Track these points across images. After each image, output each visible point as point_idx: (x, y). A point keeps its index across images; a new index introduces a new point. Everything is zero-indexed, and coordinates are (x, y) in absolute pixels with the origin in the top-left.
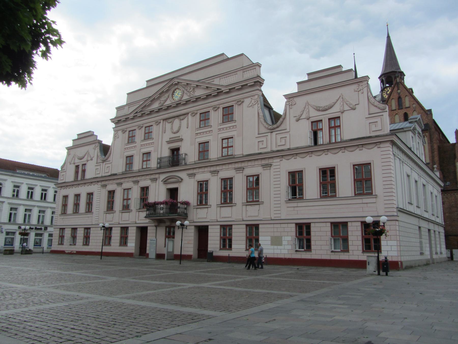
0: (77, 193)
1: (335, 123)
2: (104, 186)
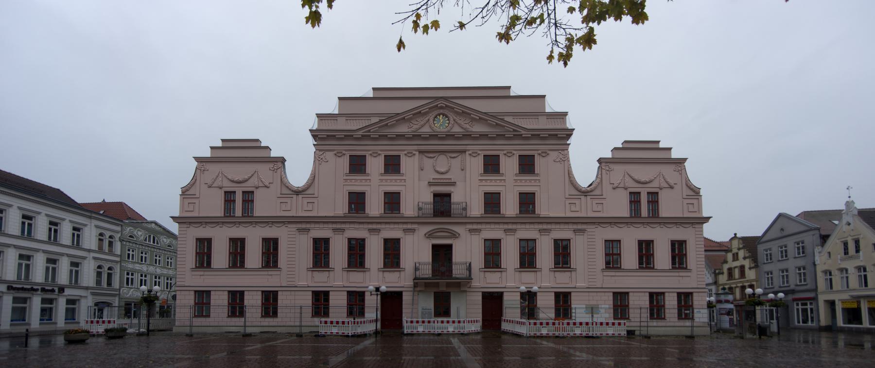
1: (248, 198)
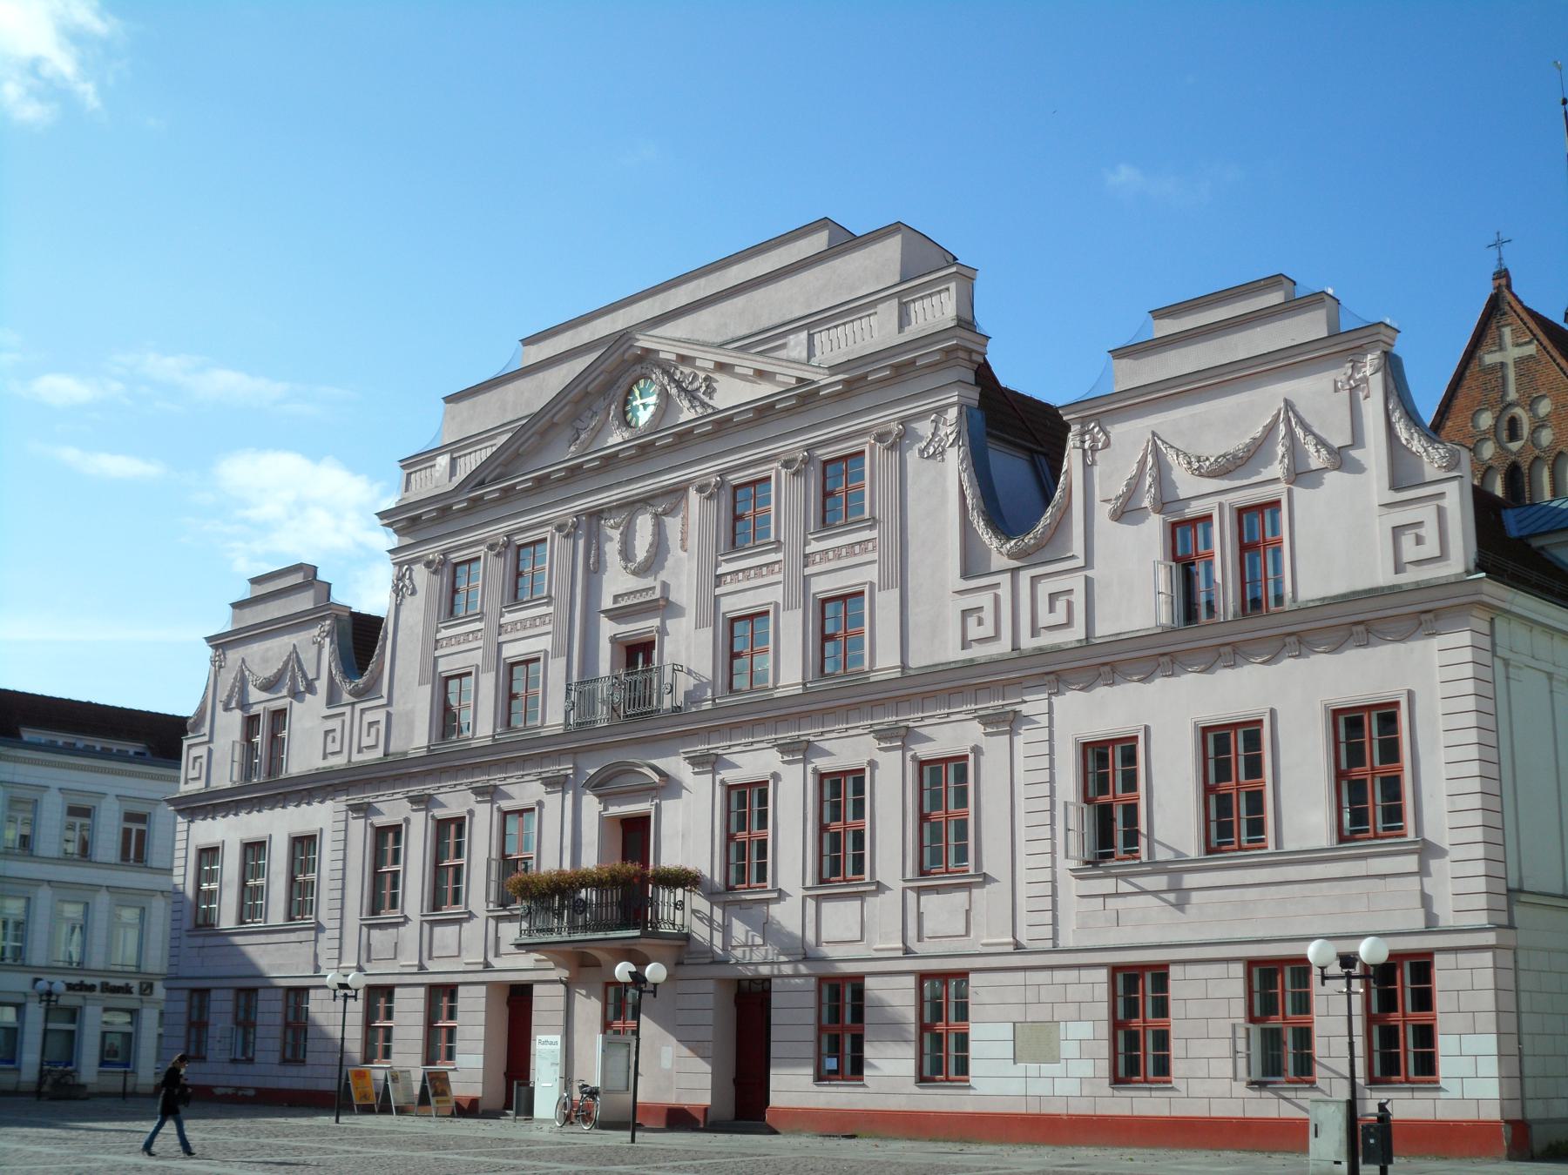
0: (254, 835)
1: (1257, 530)
2: (364, 810)
